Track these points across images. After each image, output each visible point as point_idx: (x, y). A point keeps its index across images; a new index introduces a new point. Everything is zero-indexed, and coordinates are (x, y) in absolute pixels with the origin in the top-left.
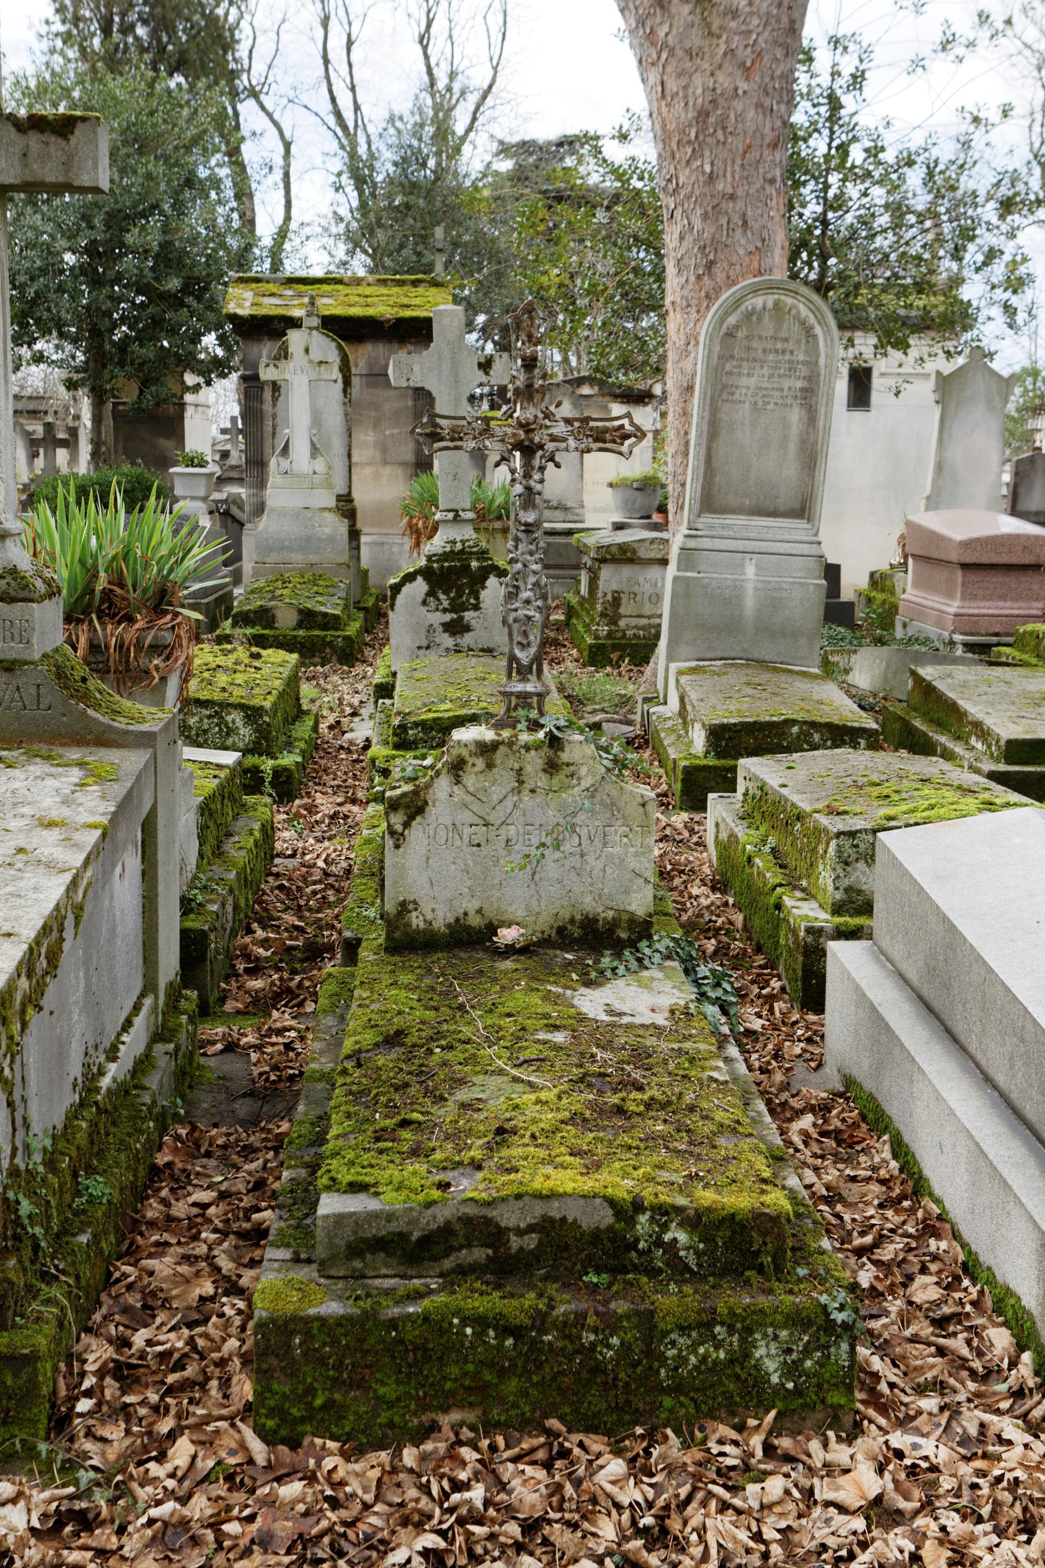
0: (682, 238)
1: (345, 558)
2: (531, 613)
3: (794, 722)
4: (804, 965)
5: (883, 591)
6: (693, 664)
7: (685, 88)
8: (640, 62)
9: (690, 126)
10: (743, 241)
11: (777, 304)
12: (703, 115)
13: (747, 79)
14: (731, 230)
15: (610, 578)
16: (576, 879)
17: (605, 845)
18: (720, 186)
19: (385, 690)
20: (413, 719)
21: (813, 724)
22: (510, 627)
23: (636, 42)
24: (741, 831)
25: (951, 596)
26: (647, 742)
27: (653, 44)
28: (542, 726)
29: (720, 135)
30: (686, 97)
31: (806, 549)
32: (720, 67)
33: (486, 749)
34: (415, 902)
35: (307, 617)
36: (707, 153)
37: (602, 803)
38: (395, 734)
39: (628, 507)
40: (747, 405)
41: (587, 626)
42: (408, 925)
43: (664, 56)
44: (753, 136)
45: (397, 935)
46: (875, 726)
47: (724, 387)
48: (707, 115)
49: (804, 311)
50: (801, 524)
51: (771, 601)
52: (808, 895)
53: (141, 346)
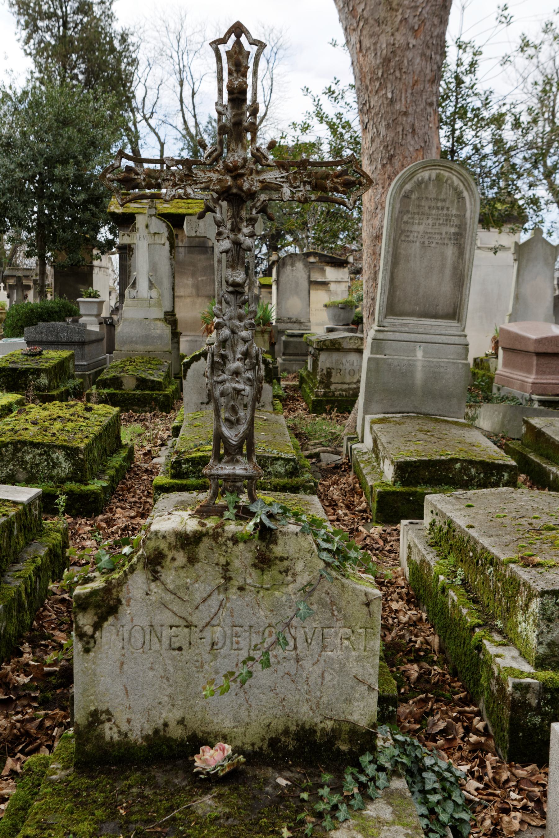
0: (372, 141)
1: (169, 348)
2: (240, 386)
3: (457, 460)
4: (512, 719)
5: (482, 369)
6: (381, 416)
7: (375, 44)
8: (346, 29)
9: (378, 68)
10: (412, 142)
11: (439, 178)
12: (386, 61)
13: (415, 37)
14: (404, 135)
15: (326, 360)
16: (291, 686)
17: (324, 648)
18: (398, 107)
19: (176, 431)
20: (186, 457)
21: (471, 462)
22: (216, 402)
23: (343, 17)
24: (431, 559)
25: (529, 372)
26: (350, 467)
27: (354, 17)
28: (253, 515)
29: (398, 74)
30: (375, 49)
31: (457, 340)
32: (398, 30)
33: (187, 542)
34: (108, 712)
35: (142, 383)
36: (389, 85)
37: (321, 602)
38: (172, 467)
39: (336, 318)
40: (418, 244)
41: (311, 389)
42: (101, 737)
43: (361, 24)
44: (419, 75)
45: (88, 748)
46: (514, 463)
47: (403, 232)
48: (389, 61)
49: (456, 181)
50: (454, 323)
51: (434, 375)
52: (508, 638)
53: (64, 231)
